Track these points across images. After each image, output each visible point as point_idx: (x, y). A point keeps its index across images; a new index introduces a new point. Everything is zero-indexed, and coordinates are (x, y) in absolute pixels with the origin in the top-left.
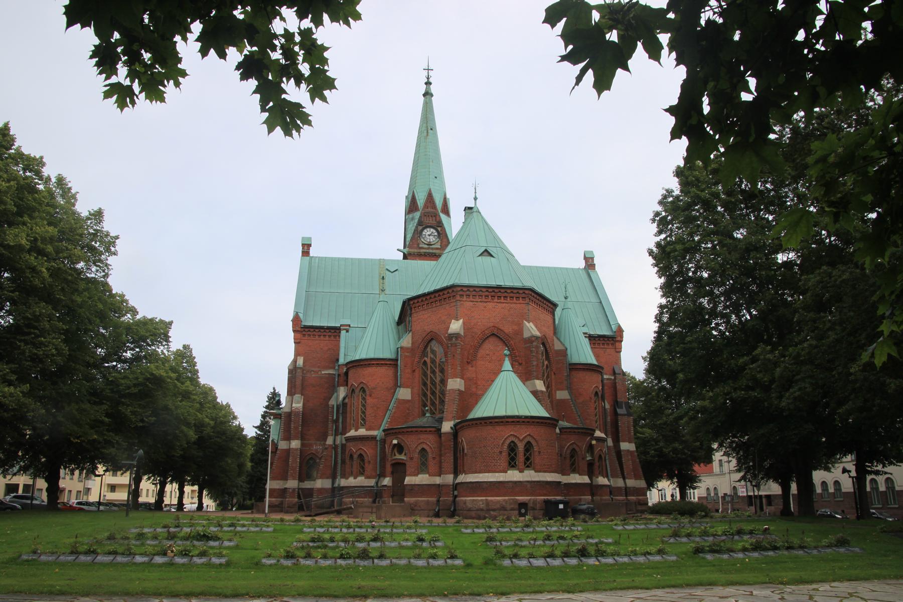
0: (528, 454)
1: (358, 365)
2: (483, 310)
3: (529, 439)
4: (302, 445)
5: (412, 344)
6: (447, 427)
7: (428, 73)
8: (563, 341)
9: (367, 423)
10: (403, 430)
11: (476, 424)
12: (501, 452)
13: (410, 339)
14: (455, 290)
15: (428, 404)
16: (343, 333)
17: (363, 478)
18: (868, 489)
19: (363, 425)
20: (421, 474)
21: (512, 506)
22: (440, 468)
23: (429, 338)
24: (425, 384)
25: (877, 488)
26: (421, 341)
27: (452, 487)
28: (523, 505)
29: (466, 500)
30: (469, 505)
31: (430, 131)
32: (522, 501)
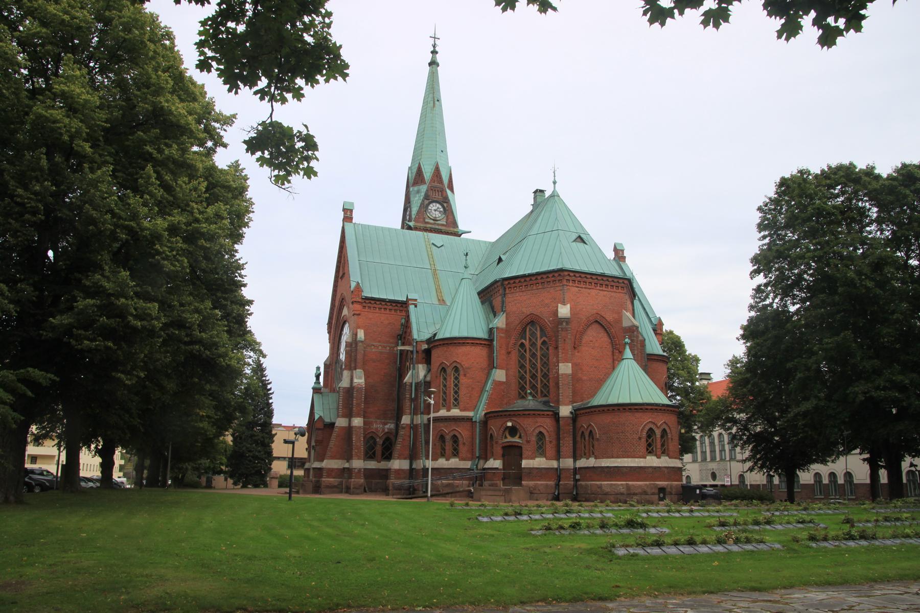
0: (650, 441)
1: (451, 344)
4: (365, 423)
6: (565, 411)
7: (435, 41)
9: (460, 403)
10: (519, 413)
11: (613, 410)
12: (640, 438)
13: (505, 320)
14: (562, 274)
16: (412, 307)
18: (904, 481)
20: (538, 457)
21: (653, 491)
23: (529, 319)
24: (522, 367)
25: (820, 482)
26: (517, 322)
27: (572, 471)
28: (662, 490)
29: (587, 485)
30: (608, 490)
31: (437, 102)
32: (661, 486)
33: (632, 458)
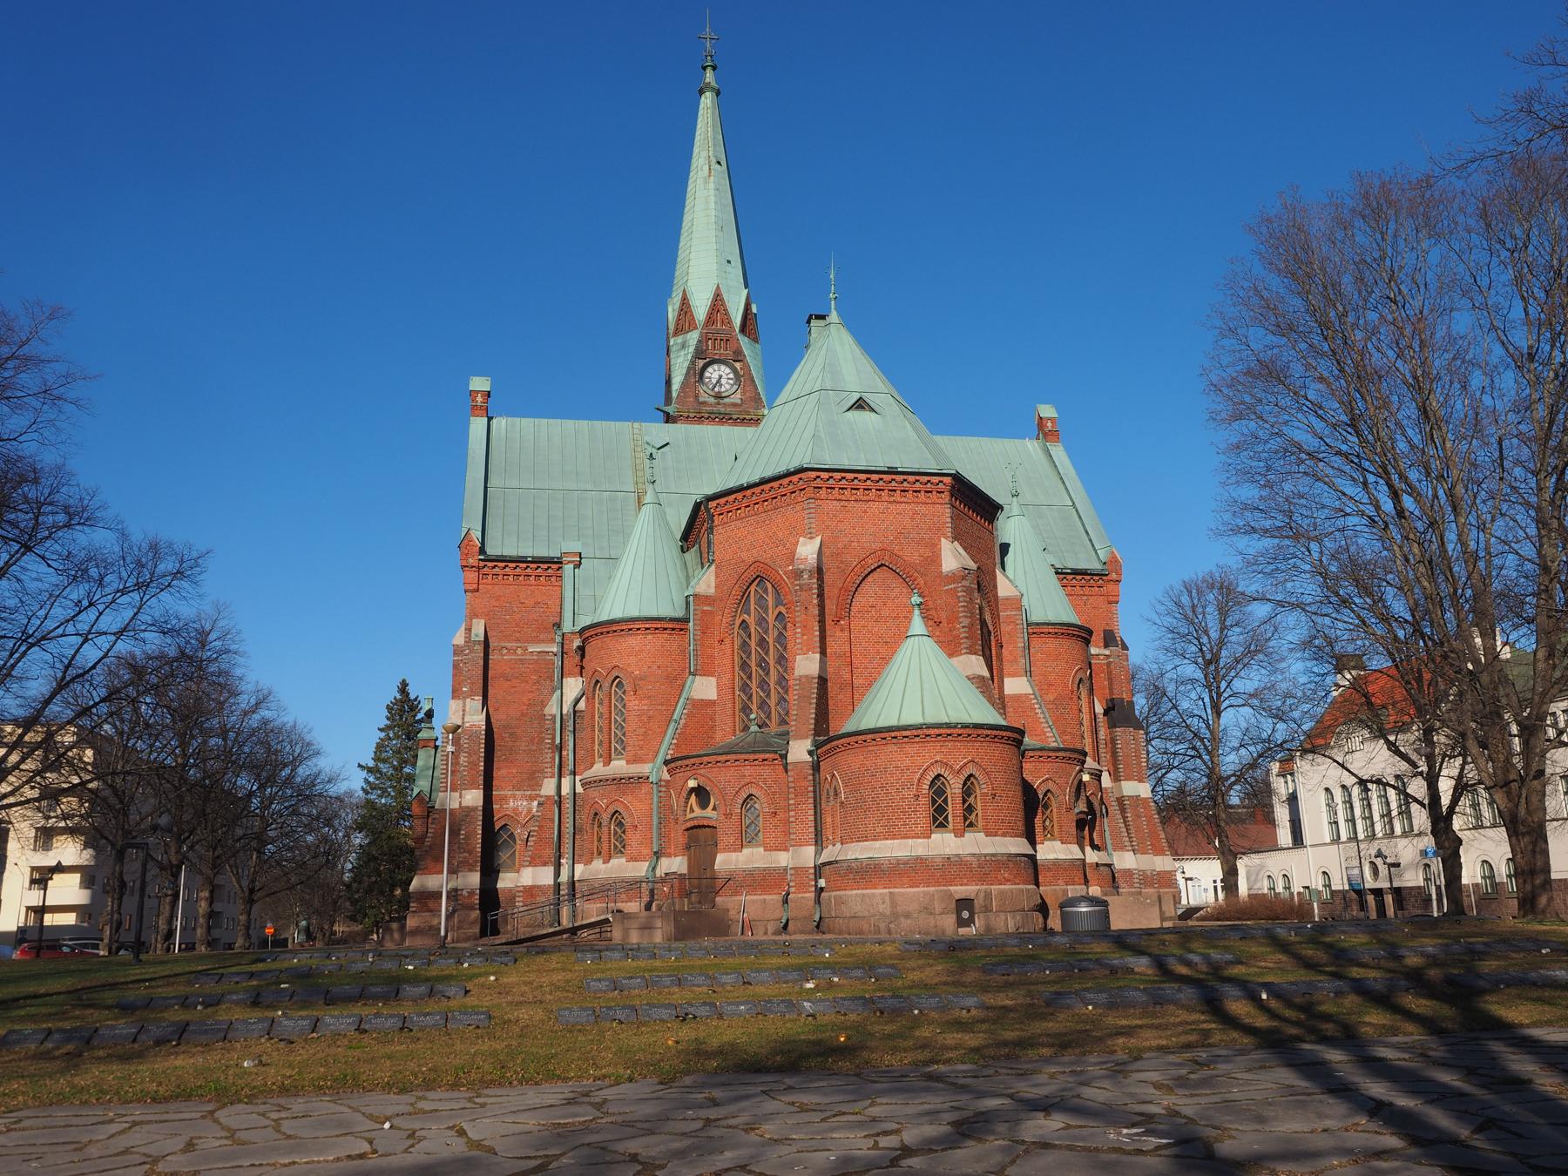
2: (861, 517)
3: (971, 769)
8: (1011, 577)
13: (713, 578)
15: (754, 707)
16: (568, 568)
17: (623, 860)
20: (747, 847)
22: (787, 833)
23: (751, 574)
27: (812, 871)
33: (902, 838)
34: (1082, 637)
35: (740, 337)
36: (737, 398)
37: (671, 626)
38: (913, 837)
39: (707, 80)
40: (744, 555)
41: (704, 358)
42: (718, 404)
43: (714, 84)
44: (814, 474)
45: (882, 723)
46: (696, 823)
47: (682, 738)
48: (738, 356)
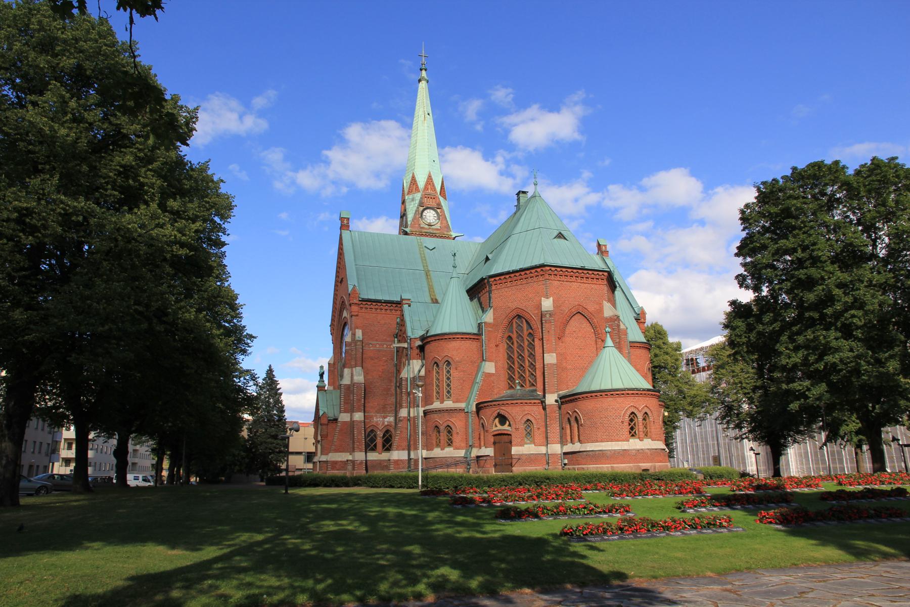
1: (442, 339)
5: (494, 319)
11: (596, 396)
14: (543, 269)
19: (449, 398)
34: (647, 348)
35: (440, 197)
36: (438, 226)
37: (473, 337)
38: (621, 441)
39: (423, 75)
40: (510, 305)
41: (423, 207)
42: (430, 228)
43: (426, 77)
44: (548, 268)
45: (603, 388)
46: (500, 432)
47: (482, 391)
48: (439, 206)
